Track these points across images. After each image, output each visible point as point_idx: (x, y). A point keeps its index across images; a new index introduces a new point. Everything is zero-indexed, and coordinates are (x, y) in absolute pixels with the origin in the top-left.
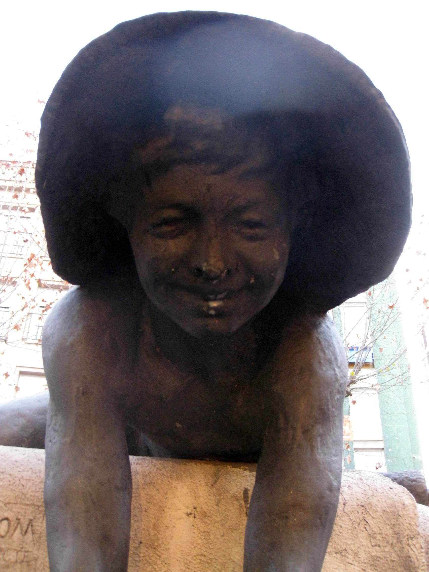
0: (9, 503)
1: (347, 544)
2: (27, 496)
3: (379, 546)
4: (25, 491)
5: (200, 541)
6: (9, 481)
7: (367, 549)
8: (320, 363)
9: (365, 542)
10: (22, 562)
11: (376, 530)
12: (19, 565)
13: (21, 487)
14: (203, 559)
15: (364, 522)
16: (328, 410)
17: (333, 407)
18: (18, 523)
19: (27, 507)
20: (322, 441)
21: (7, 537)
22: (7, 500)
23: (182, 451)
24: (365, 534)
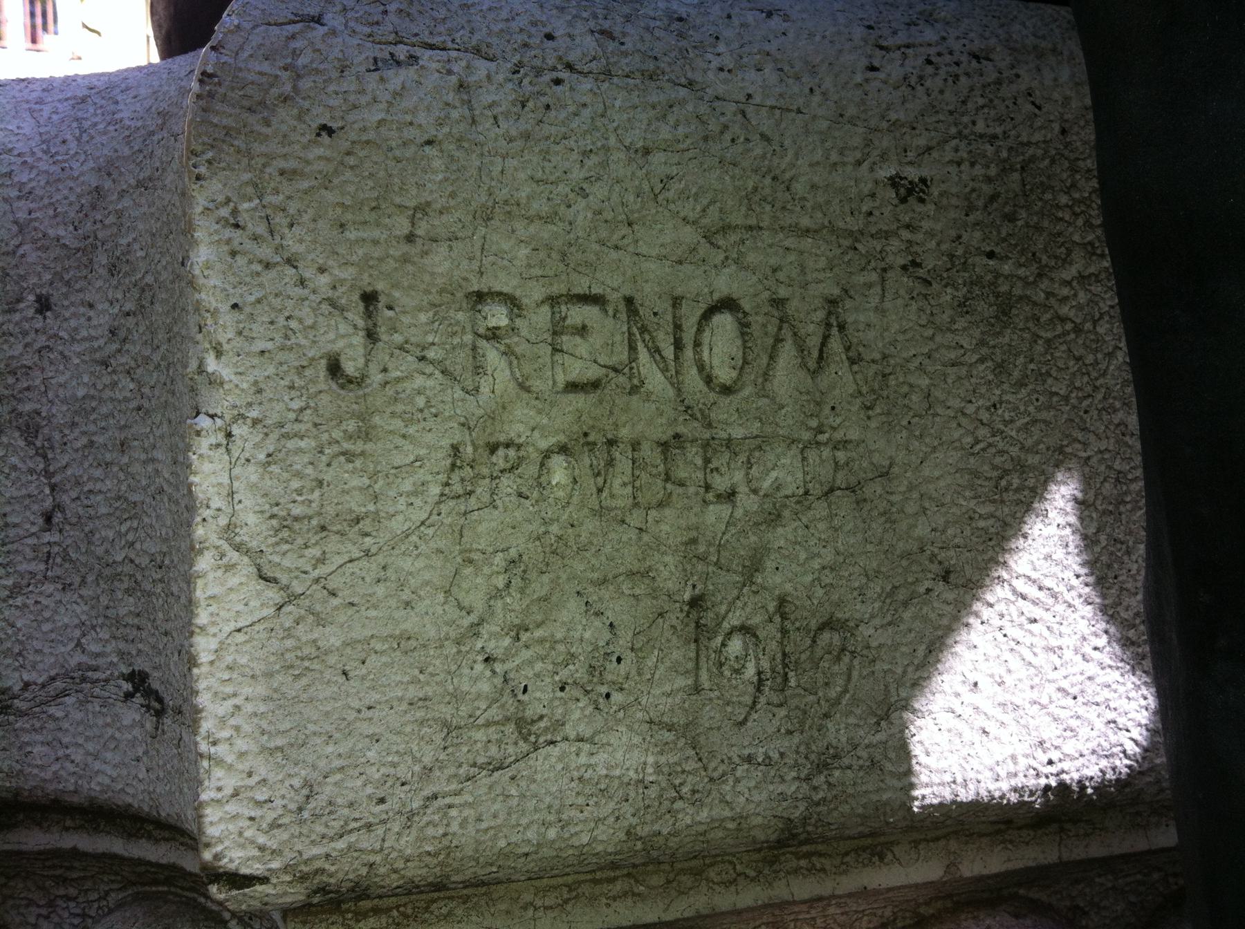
12: (820, 509)
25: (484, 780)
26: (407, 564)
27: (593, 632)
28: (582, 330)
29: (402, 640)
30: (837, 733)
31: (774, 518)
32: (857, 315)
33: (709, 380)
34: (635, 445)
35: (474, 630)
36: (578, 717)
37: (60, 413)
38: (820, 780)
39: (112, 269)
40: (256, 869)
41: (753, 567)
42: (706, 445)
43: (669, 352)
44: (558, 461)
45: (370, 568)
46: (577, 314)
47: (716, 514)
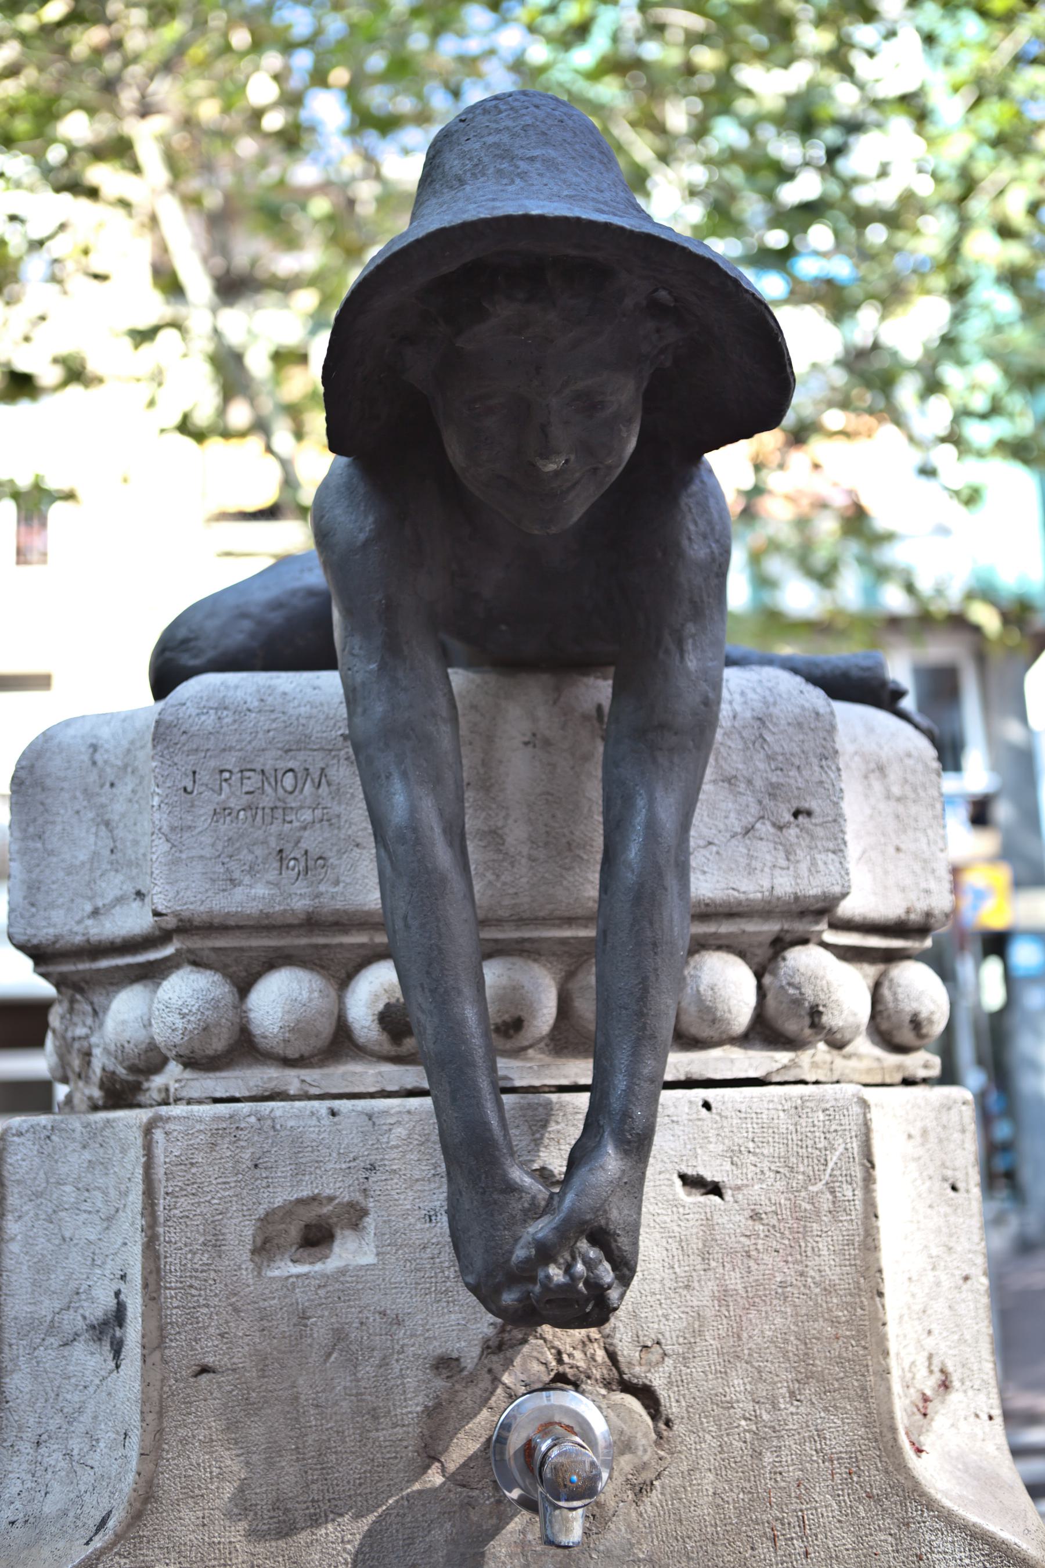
0: (290, 750)
1: (737, 769)
2: (313, 738)
3: (781, 770)
4: (308, 732)
5: (544, 777)
6: (284, 722)
7: (765, 775)
8: (690, 539)
9: (761, 766)
10: (322, 820)
11: (777, 749)
12: (318, 826)
13: (301, 728)
14: (550, 798)
15: (760, 740)
16: (702, 601)
17: (709, 597)
18: (308, 775)
19: (315, 753)
20: (694, 644)
21: (296, 793)
22: (287, 747)
23: (509, 663)
24: (762, 755)
25: (221, 894)
26: (203, 839)
27: (250, 857)
28: (249, 778)
29: (201, 857)
30: (322, 888)
31: (305, 828)
32: (331, 772)
33: (286, 791)
34: (263, 809)
35: (219, 856)
36: (247, 880)
37: (117, 818)
38: (317, 901)
39: (133, 772)
40: (164, 911)
41: (298, 842)
42: (284, 809)
43: (273, 783)
44: (242, 813)
45: (194, 839)
46: (247, 774)
47: (287, 826)
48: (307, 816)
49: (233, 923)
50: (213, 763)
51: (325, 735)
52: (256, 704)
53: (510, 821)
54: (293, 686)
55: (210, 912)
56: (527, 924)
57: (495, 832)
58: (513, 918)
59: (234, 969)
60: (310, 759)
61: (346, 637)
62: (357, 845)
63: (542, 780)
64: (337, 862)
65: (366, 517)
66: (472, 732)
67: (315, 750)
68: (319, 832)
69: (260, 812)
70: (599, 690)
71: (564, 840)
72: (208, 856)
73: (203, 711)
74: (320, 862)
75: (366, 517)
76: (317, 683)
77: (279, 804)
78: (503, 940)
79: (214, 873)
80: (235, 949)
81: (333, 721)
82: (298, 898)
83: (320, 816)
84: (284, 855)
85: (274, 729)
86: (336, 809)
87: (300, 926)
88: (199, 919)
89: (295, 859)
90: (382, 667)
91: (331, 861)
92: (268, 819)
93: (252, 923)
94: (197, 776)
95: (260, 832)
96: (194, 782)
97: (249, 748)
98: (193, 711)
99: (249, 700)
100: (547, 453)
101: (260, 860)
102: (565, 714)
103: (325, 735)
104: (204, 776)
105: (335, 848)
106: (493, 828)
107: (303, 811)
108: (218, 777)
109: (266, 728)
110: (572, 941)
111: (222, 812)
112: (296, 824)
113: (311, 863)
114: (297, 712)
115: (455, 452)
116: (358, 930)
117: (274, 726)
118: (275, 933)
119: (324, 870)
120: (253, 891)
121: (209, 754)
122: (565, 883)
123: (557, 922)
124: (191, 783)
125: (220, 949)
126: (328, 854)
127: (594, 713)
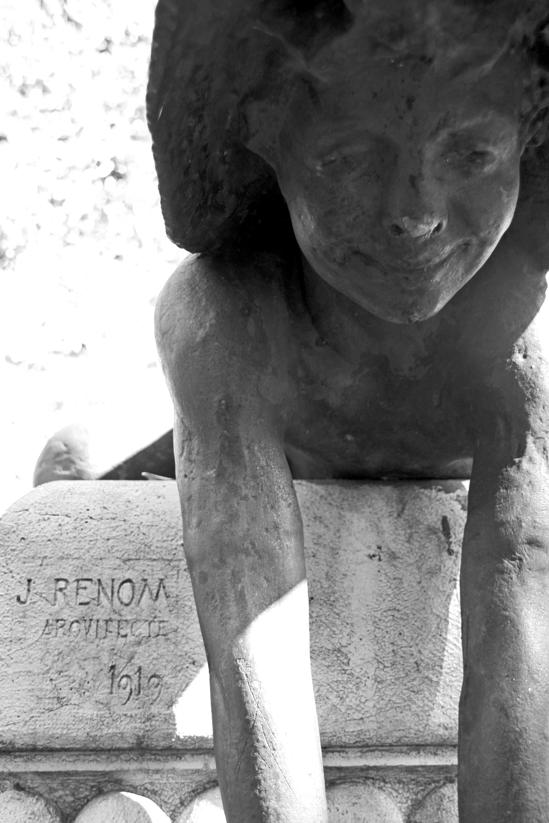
0: (129, 560)
2: (153, 548)
5: (390, 592)
12: (153, 640)
13: (141, 537)
14: (396, 614)
19: (155, 563)
21: (133, 605)
22: (126, 556)
27: (81, 674)
28: (85, 588)
30: (154, 710)
31: (139, 643)
33: (122, 603)
34: (98, 621)
35: (48, 672)
36: (75, 698)
38: (148, 723)
43: (110, 594)
44: (75, 625)
46: (83, 584)
47: (122, 640)
48: (143, 629)
49: (58, 747)
50: (49, 572)
51: (165, 544)
52: (99, 511)
53: (355, 639)
54: (137, 494)
55: (34, 733)
56: (373, 751)
57: (339, 651)
58: (358, 744)
59: (61, 793)
60: (148, 569)
61: (183, 441)
62: (194, 663)
63: (388, 595)
64: (172, 681)
65: (207, 312)
66: (315, 544)
67: (155, 560)
68: (154, 647)
69: (94, 625)
70: (452, 503)
71: (412, 661)
72: (36, 671)
73: (45, 517)
74: (155, 680)
75: (207, 312)
76: (163, 491)
77: (115, 617)
78: (347, 768)
79: (41, 690)
80: (59, 773)
81: (174, 530)
82: (128, 720)
83: (156, 630)
84: (116, 672)
85: (114, 538)
86: (175, 623)
87: (131, 749)
88: (21, 742)
89: (127, 676)
90: (220, 475)
91: (166, 679)
92: (102, 633)
93: (78, 746)
94: (32, 585)
95: (93, 646)
96: (29, 590)
97: (87, 557)
98: (34, 517)
99: (91, 507)
100: (417, 214)
101: (89, 678)
102: (410, 527)
103: (165, 544)
104: (38, 586)
105: (170, 666)
106: (338, 646)
107: (139, 624)
108: (53, 586)
109: (105, 536)
110: (420, 769)
111: (55, 623)
112: (130, 638)
113: (144, 681)
114: (137, 521)
115: (304, 226)
116: (193, 755)
117: (114, 534)
118: (104, 757)
119: (157, 690)
120: (81, 711)
121: (45, 562)
122: (414, 707)
123: (405, 749)
124: (26, 591)
125: (44, 773)
126: (162, 672)
127: (439, 525)
